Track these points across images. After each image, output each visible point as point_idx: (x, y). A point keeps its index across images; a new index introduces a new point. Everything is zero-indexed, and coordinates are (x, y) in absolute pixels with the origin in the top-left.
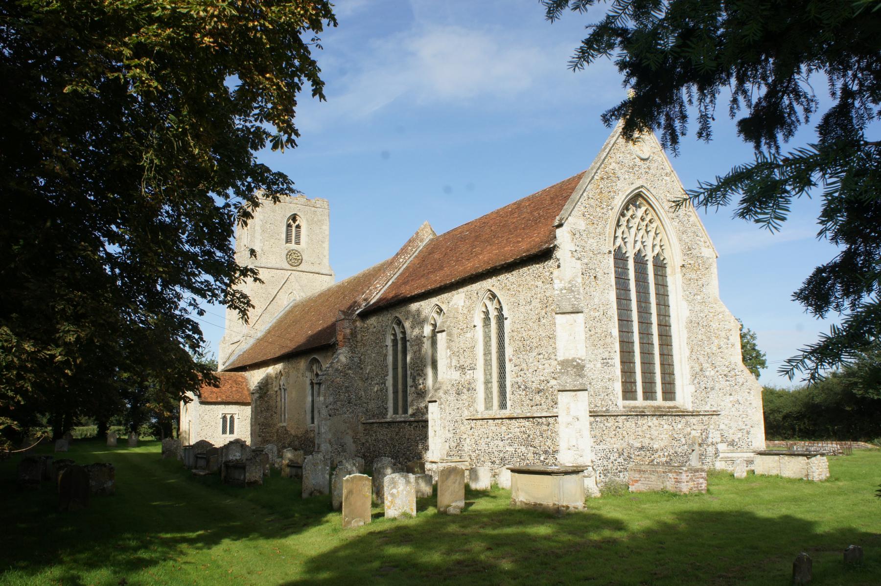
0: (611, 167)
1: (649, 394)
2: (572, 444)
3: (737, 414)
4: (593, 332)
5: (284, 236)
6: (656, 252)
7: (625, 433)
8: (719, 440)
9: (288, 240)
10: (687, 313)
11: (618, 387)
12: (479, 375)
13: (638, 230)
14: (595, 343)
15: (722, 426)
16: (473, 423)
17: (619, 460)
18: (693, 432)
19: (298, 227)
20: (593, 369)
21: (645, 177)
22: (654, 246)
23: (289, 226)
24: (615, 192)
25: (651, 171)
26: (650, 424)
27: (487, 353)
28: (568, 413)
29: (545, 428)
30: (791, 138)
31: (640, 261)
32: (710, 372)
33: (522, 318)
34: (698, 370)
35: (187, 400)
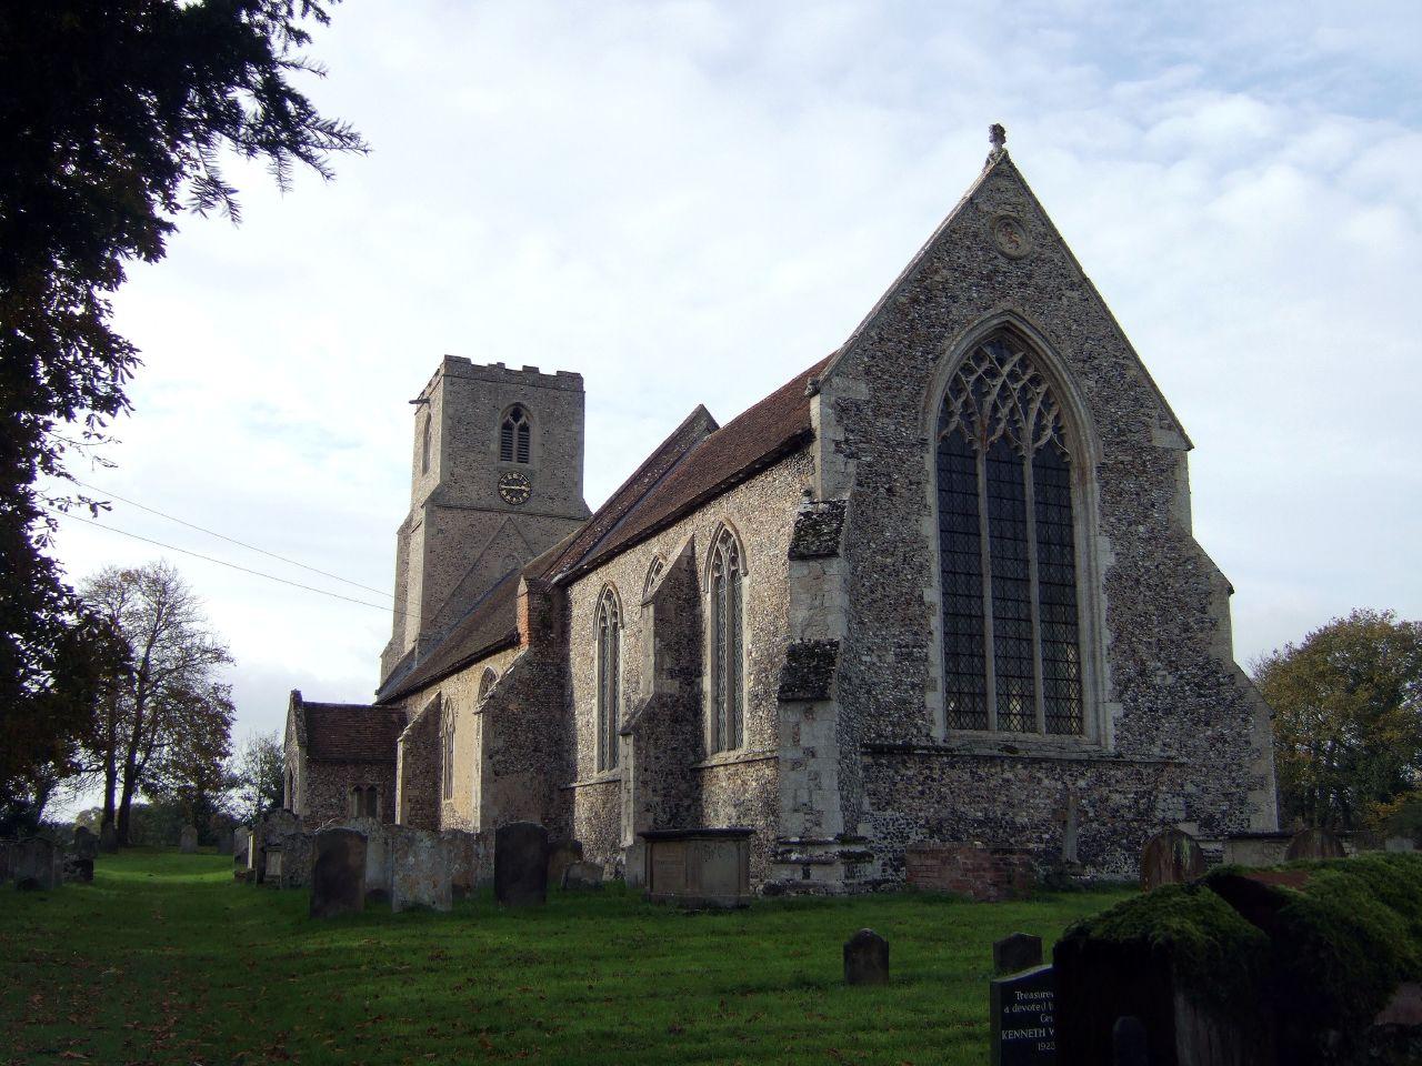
2: (800, 800)
4: (878, 595)
8: (1181, 815)
9: (506, 452)
18: (1116, 797)
19: (525, 428)
21: (1017, 293)
23: (507, 427)
24: (945, 326)
30: (364, 139)
31: (1005, 458)
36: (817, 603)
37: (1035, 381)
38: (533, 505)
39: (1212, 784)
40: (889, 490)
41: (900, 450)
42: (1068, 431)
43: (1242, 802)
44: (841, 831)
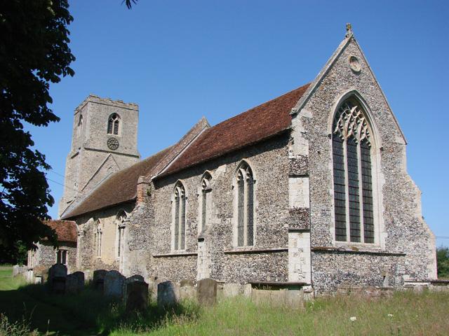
0: (333, 76)
1: (355, 237)
2: (297, 268)
3: (418, 254)
5: (106, 128)
6: (363, 138)
7: (336, 264)
8: (404, 272)
9: (109, 131)
10: (384, 182)
11: (333, 230)
12: (235, 221)
13: (351, 121)
14: (317, 199)
15: (407, 263)
16: (229, 256)
17: (331, 283)
19: (117, 122)
20: (315, 217)
22: (362, 133)
23: (110, 122)
25: (361, 81)
26: (355, 258)
27: (241, 206)
28: (295, 246)
29: (280, 258)
31: (351, 140)
32: (399, 224)
33: (266, 180)
34: (390, 221)
35: (35, 248)
36: (300, 193)
37: (360, 116)
38: (119, 150)
39: (415, 261)
40: (319, 152)
41: (322, 138)
42: (371, 134)
43: (425, 268)
44: (30, 253)
